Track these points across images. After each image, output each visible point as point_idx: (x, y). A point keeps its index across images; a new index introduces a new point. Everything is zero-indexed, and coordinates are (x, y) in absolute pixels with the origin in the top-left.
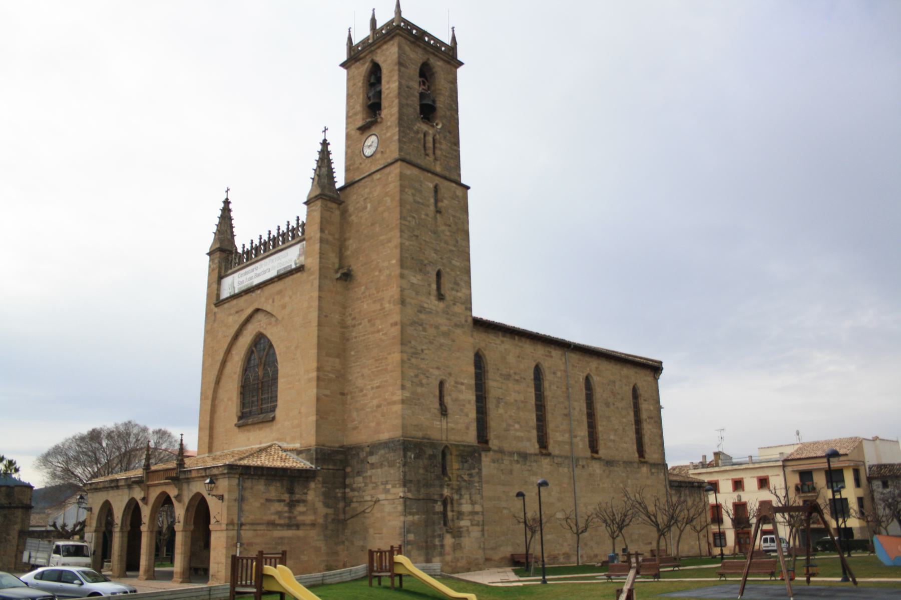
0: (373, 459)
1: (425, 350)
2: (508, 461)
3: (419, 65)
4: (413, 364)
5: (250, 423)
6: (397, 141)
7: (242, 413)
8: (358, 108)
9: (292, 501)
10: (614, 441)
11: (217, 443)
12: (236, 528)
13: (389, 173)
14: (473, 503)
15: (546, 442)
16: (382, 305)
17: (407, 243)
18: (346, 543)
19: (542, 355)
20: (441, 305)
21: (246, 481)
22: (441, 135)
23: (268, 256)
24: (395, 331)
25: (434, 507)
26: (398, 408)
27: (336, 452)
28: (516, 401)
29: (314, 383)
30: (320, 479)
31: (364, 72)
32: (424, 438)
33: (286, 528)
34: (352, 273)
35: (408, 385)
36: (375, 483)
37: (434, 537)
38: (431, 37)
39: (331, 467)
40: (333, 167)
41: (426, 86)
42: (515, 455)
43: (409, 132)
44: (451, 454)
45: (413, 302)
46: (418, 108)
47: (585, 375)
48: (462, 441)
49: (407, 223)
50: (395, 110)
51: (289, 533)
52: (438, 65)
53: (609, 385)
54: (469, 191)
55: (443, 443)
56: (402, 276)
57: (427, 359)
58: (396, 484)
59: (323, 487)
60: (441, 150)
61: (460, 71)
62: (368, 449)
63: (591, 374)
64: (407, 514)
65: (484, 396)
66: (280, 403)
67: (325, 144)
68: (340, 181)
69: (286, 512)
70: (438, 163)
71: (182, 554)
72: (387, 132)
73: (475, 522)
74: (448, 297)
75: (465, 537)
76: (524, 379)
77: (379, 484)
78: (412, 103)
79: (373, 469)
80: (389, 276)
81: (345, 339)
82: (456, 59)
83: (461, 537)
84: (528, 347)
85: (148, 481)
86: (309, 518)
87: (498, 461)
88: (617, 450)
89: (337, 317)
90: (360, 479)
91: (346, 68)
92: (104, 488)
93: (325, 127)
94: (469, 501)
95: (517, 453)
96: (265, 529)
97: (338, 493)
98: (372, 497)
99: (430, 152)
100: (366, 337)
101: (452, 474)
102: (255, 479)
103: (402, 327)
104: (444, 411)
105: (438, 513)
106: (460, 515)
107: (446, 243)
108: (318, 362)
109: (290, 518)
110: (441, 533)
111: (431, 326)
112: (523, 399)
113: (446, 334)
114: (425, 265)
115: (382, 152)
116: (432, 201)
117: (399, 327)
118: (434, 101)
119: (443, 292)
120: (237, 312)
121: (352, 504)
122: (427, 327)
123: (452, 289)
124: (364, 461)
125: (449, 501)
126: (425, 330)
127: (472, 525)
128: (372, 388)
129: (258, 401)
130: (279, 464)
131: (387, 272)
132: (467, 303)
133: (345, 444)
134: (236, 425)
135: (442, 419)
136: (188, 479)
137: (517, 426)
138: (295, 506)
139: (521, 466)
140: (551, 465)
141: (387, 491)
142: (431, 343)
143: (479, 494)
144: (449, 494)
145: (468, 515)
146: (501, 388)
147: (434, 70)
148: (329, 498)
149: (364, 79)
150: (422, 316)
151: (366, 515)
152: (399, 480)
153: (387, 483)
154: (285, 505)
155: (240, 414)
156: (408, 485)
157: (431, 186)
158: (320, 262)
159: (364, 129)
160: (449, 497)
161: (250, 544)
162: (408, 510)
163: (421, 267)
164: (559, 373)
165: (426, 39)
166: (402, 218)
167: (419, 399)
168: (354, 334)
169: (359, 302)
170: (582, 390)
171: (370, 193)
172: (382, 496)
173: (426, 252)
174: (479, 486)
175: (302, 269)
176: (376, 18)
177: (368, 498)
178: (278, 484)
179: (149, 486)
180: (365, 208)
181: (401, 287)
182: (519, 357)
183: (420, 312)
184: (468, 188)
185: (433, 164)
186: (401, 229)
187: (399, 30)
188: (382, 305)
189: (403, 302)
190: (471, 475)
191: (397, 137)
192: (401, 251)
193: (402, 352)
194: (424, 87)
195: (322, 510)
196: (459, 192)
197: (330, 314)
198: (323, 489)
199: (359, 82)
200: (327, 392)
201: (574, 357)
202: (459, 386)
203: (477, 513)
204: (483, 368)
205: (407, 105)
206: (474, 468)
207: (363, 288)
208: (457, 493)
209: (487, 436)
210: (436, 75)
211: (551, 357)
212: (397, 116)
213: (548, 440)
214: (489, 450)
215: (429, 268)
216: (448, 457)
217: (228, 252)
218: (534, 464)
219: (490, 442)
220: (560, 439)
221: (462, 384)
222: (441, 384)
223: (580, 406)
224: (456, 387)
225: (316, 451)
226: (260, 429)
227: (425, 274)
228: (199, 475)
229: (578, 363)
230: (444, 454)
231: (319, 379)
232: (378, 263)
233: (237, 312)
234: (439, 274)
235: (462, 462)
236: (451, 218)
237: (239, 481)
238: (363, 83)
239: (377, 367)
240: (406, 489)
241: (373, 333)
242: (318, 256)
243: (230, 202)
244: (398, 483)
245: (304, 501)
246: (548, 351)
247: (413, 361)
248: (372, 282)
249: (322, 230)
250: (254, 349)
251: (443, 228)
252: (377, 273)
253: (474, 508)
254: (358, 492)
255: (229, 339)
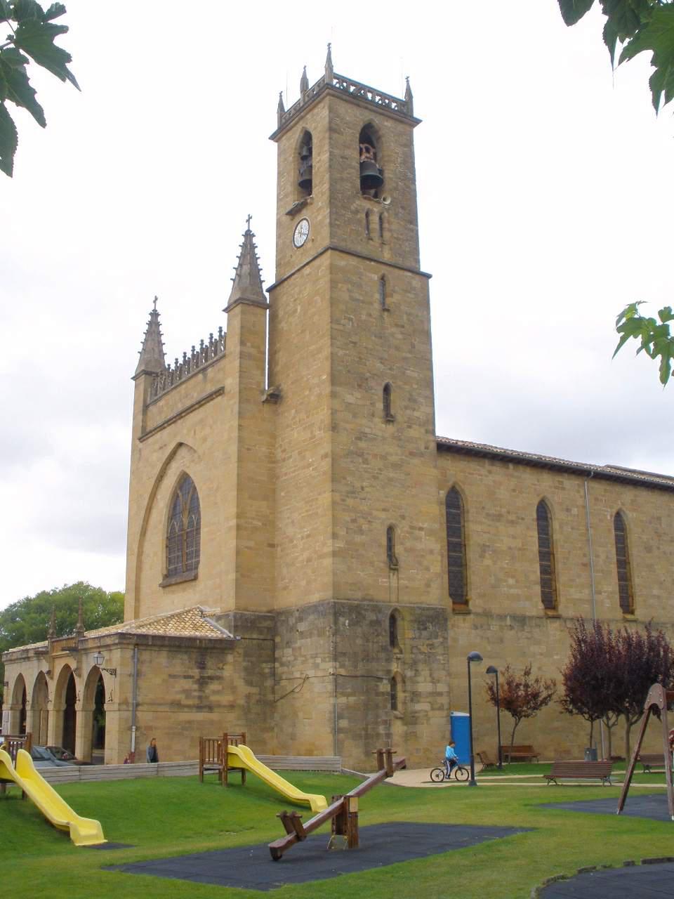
0: (302, 627)
1: (366, 487)
2: (498, 627)
3: (359, 129)
4: (348, 506)
5: (173, 583)
6: (328, 225)
7: (168, 571)
8: (289, 188)
9: (202, 677)
10: (659, 597)
11: (143, 609)
12: (131, 709)
13: (319, 267)
14: (434, 681)
15: (556, 600)
16: (312, 432)
17: (341, 353)
18: (276, 730)
19: (550, 487)
20: (391, 429)
21: (144, 652)
22: (390, 212)
23: (192, 377)
24: (326, 465)
25: (377, 686)
26: (328, 561)
27: (265, 618)
28: (510, 548)
29: (234, 533)
30: (241, 651)
31: (294, 144)
32: (364, 599)
33: (194, 710)
34: (282, 393)
35: (342, 532)
36: (305, 656)
37: (377, 723)
38: (367, 89)
39: (255, 636)
40: (258, 263)
41: (372, 154)
42: (508, 618)
43: (344, 212)
44: (403, 619)
45: (348, 426)
46: (358, 182)
47: (614, 511)
48: (421, 603)
49: (341, 328)
50: (326, 186)
51: (200, 716)
52: (386, 126)
53: (650, 523)
54: (430, 280)
55: (391, 606)
56: (333, 395)
57: (369, 499)
58: (325, 658)
59: (244, 661)
60: (390, 231)
61: (416, 130)
62: (297, 614)
63: (624, 509)
64: (338, 695)
65: (463, 543)
66: (202, 558)
67: (249, 235)
68: (268, 277)
69: (195, 690)
70: (386, 248)
71: (82, 737)
72: (318, 215)
73: (436, 706)
74: (399, 418)
75: (423, 724)
76: (523, 519)
77: (308, 657)
78: (349, 176)
79: (302, 639)
80: (319, 396)
81: (273, 476)
82: (412, 116)
83: (416, 724)
84: (528, 477)
85: (53, 652)
86: (226, 699)
87: (482, 627)
88: (664, 609)
89: (264, 449)
90: (289, 651)
91: (276, 141)
92: (17, 659)
93: (249, 215)
94: (429, 679)
95: (510, 616)
96: (168, 710)
97: (264, 668)
98: (302, 674)
99: (375, 235)
100: (297, 473)
101: (405, 644)
102: (155, 651)
103: (333, 459)
104: (393, 563)
105: (383, 694)
106: (415, 696)
107: (397, 348)
108: (238, 507)
109: (200, 698)
110: (388, 719)
111: (375, 456)
112: (520, 545)
113: (396, 466)
114: (367, 379)
115: (313, 240)
116: (377, 296)
117: (329, 460)
118: (381, 171)
119: (392, 412)
120: (161, 448)
121: (281, 681)
122: (370, 457)
123: (406, 408)
124: (292, 629)
125: (399, 679)
126: (366, 462)
127: (433, 709)
128: (302, 538)
129: (182, 556)
130: (187, 633)
131: (317, 391)
132: (430, 422)
133: (275, 608)
134: (160, 585)
135: (391, 574)
136: (85, 649)
137: (511, 581)
138: (207, 683)
139: (517, 632)
140: (562, 631)
141: (316, 666)
142: (375, 478)
143: (444, 669)
144: (399, 670)
145: (427, 697)
146: (489, 533)
147: (380, 133)
148: (252, 675)
149: (294, 153)
150: (362, 444)
151: (296, 695)
152: (329, 653)
153: (315, 656)
154: (196, 682)
155: (165, 572)
156: (341, 659)
157: (376, 277)
158: (240, 383)
159: (294, 213)
160: (400, 673)
161: (150, 728)
162: (339, 690)
163: (361, 383)
164: (576, 509)
165: (370, 96)
166: (334, 320)
167: (357, 550)
168: (284, 470)
169: (289, 429)
170: (609, 530)
171: (300, 292)
172: (311, 673)
173: (368, 363)
174: (444, 660)
175: (221, 392)
176: (308, 77)
177: (297, 675)
178: (185, 657)
179: (54, 658)
180: (295, 311)
181: (332, 409)
182: (514, 490)
183: (359, 439)
184: (429, 276)
185: (380, 249)
186: (331, 335)
187: (330, 89)
188: (312, 432)
189: (334, 428)
190: (431, 646)
191: (328, 221)
192: (332, 364)
193: (333, 491)
194: (368, 155)
195: (243, 689)
196: (416, 282)
197: (255, 446)
198: (245, 664)
199: (290, 156)
200: (252, 544)
201: (599, 488)
202: (417, 532)
203: (440, 694)
204: (462, 508)
205: (342, 179)
206: (436, 637)
207: (293, 411)
208: (411, 669)
209: (467, 595)
210: (383, 139)
211: (563, 489)
212: (327, 194)
213: (558, 598)
214: (469, 613)
215: (372, 383)
216: (399, 623)
217: (154, 375)
218: (537, 630)
219: (471, 603)
220: (577, 596)
221: (421, 529)
222: (390, 530)
223: (607, 552)
224: (411, 533)
225: (235, 617)
226: (184, 590)
227: (366, 391)
228: (95, 645)
229: (603, 496)
230: (393, 619)
231: (239, 527)
232: (308, 380)
233: (161, 448)
234: (387, 390)
235: (419, 629)
236: (405, 317)
237: (134, 653)
238: (294, 158)
239: (307, 511)
240: (338, 663)
241: (304, 468)
242: (237, 374)
243: (158, 315)
244: (328, 657)
245: (219, 678)
246: (559, 481)
247: (350, 502)
248: (302, 403)
249: (242, 343)
250: (179, 492)
251: (394, 330)
252: (307, 393)
253: (436, 689)
254: (288, 666)
255: (153, 481)
